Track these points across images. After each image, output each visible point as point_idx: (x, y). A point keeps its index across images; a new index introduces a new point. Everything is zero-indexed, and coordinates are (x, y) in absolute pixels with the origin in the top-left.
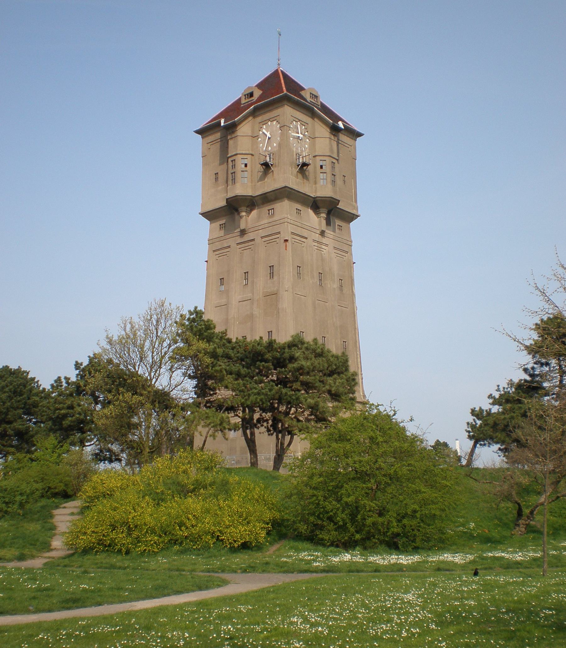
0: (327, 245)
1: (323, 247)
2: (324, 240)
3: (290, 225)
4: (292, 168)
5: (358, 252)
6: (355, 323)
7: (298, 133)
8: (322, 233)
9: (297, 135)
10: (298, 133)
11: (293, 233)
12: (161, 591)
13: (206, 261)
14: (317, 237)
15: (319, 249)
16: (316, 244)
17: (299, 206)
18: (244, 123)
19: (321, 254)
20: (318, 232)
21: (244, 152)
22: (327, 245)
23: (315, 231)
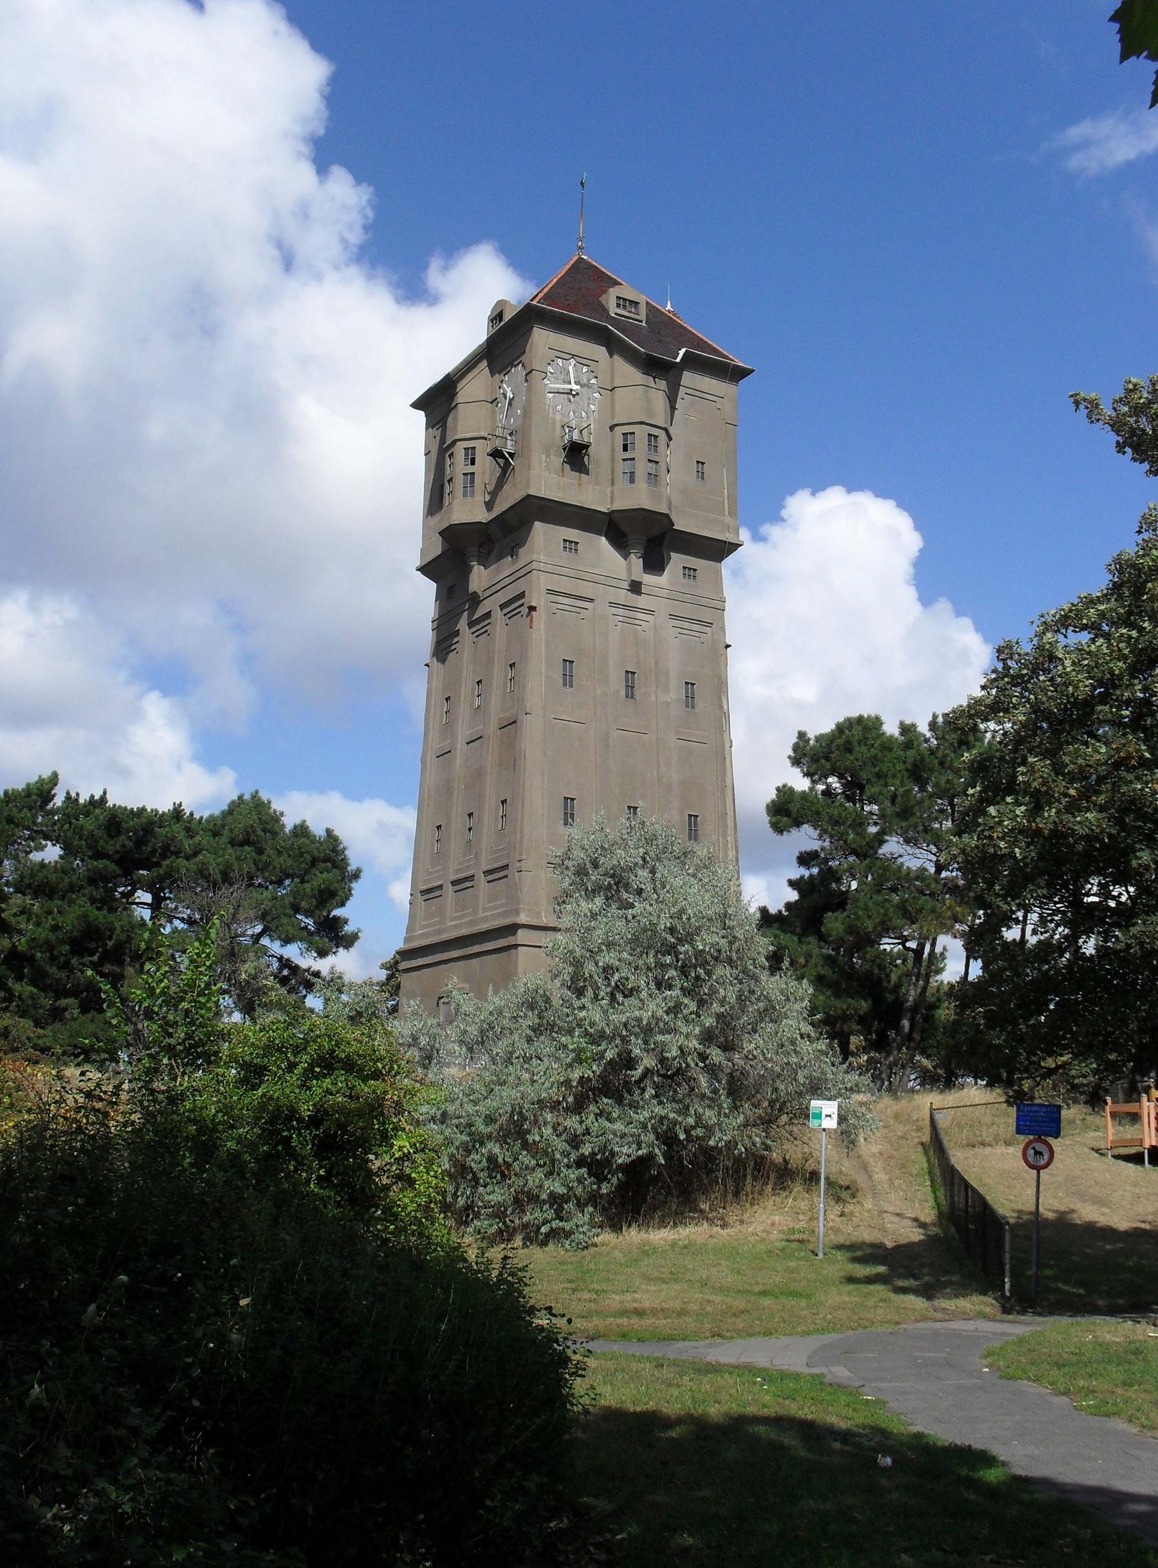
0: (651, 612)
1: (640, 616)
2: (642, 601)
3: (543, 576)
4: (548, 456)
5: (738, 620)
6: (724, 774)
7: (570, 383)
8: (636, 587)
9: (569, 387)
10: (570, 383)
11: (551, 592)
12: (1001, 1246)
13: (728, 646)
14: (624, 596)
15: (630, 621)
16: (621, 612)
17: (573, 534)
18: (470, 376)
19: (636, 631)
20: (626, 585)
21: (468, 435)
22: (651, 612)
23: (614, 583)
